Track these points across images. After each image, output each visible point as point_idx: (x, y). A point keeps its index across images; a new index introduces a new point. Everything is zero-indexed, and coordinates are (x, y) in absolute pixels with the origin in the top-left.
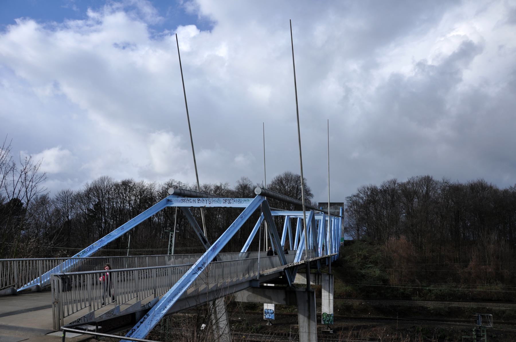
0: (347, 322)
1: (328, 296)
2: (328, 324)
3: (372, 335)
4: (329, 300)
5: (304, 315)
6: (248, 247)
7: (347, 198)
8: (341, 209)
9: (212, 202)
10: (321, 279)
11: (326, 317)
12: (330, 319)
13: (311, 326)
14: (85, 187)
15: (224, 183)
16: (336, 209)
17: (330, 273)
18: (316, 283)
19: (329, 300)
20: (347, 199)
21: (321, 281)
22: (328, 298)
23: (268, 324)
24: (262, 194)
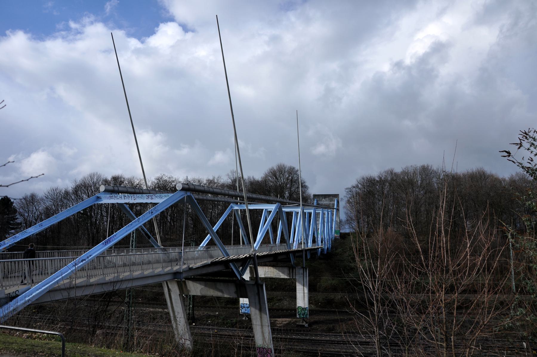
0: (325, 315)
1: (303, 290)
2: (303, 317)
3: (348, 328)
4: (304, 293)
5: (256, 308)
6: (208, 241)
7: (347, 189)
8: (336, 201)
9: (136, 198)
10: (295, 273)
11: (301, 311)
12: (305, 313)
13: (263, 319)
14: (73, 184)
15: (216, 177)
16: (331, 201)
17: (305, 266)
18: (290, 276)
19: (304, 293)
20: (347, 191)
21: (295, 274)
22: (302, 292)
23: (244, 318)
24: (183, 189)
